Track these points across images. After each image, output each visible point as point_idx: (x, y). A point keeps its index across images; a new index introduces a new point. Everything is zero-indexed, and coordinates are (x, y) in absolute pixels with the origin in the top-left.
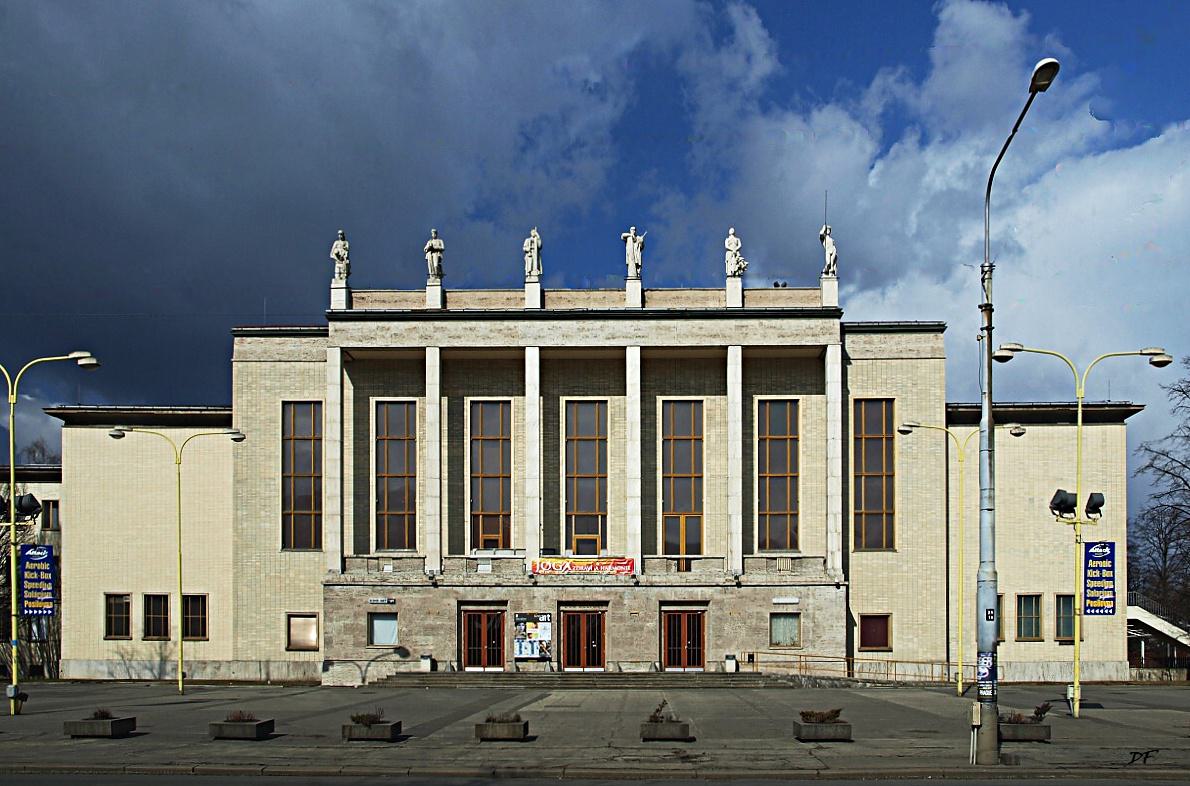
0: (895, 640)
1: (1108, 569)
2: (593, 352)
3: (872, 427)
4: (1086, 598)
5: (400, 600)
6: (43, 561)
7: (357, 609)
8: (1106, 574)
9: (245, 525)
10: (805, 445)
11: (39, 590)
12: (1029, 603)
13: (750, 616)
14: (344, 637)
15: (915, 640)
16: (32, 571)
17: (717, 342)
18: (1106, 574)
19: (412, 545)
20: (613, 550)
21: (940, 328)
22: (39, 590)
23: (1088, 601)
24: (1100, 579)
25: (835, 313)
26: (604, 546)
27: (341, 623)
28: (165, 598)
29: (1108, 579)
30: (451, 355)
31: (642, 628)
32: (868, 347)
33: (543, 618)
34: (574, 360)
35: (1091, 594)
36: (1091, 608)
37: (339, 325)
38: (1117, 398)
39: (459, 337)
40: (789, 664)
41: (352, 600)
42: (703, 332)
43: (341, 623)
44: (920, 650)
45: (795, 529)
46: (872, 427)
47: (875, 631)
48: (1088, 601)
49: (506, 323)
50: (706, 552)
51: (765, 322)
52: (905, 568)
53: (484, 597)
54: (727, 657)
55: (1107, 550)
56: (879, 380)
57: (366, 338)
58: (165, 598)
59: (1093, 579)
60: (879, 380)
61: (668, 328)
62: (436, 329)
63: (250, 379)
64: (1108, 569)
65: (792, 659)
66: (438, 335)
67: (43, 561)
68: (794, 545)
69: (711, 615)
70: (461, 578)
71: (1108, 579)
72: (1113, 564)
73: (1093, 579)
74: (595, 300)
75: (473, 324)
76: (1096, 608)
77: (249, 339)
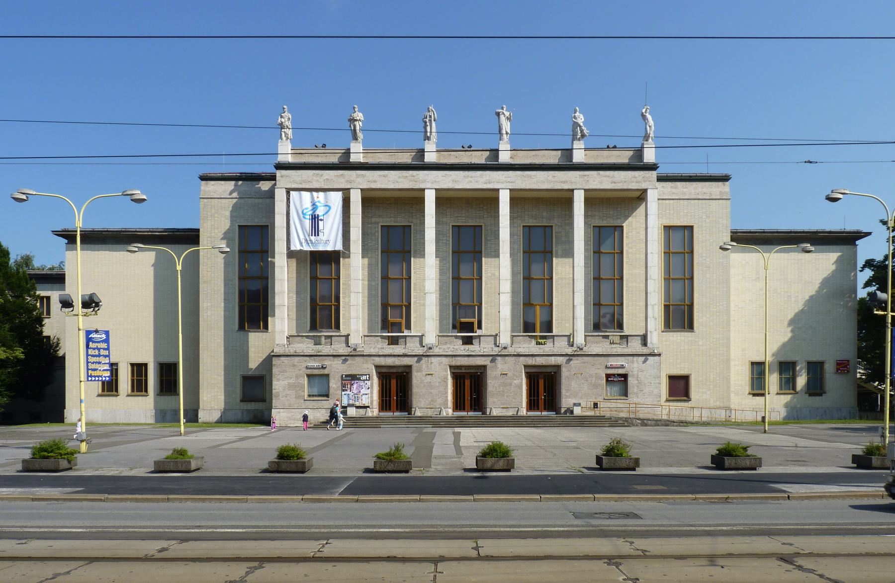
0: (693, 393)
1: (104, 349)
2: (491, 192)
3: (680, 242)
4: (88, 369)
5: (331, 365)
6: (102, 341)
7: (298, 372)
8: (103, 352)
9: (209, 313)
10: (628, 257)
11: (99, 363)
12: (139, 370)
13: (591, 376)
14: (288, 392)
15: (708, 392)
16: (94, 349)
17: (566, 187)
18: (103, 352)
19: (338, 327)
20: (486, 329)
21: (725, 179)
22: (99, 363)
23: (90, 372)
24: (99, 356)
25: (652, 167)
26: (480, 327)
27: (286, 382)
28: (146, 365)
29: (105, 356)
30: (517, 195)
31: (510, 384)
32: (674, 190)
33: (364, 378)
34: (458, 198)
35: (91, 366)
36: (91, 376)
37: (284, 172)
38: (851, 227)
39: (375, 181)
40: (620, 410)
41: (294, 365)
42: (556, 179)
43: (286, 382)
44: (712, 400)
45: (622, 315)
46: (680, 242)
47: (680, 387)
48: (90, 372)
49: (411, 172)
50: (555, 331)
51: (602, 173)
52: (701, 343)
53: (644, 362)
54: (575, 405)
55: (104, 336)
56: (682, 214)
57: (305, 182)
58: (146, 365)
59: (93, 356)
60: (682, 214)
61: (530, 176)
62: (358, 176)
63: (213, 211)
64: (104, 349)
65: (622, 406)
66: (359, 180)
67: (102, 341)
68: (620, 326)
69: (564, 373)
70: (377, 350)
71: (105, 356)
72: (108, 346)
73: (93, 356)
74: (475, 156)
75: (386, 172)
76: (95, 377)
77: (212, 182)
